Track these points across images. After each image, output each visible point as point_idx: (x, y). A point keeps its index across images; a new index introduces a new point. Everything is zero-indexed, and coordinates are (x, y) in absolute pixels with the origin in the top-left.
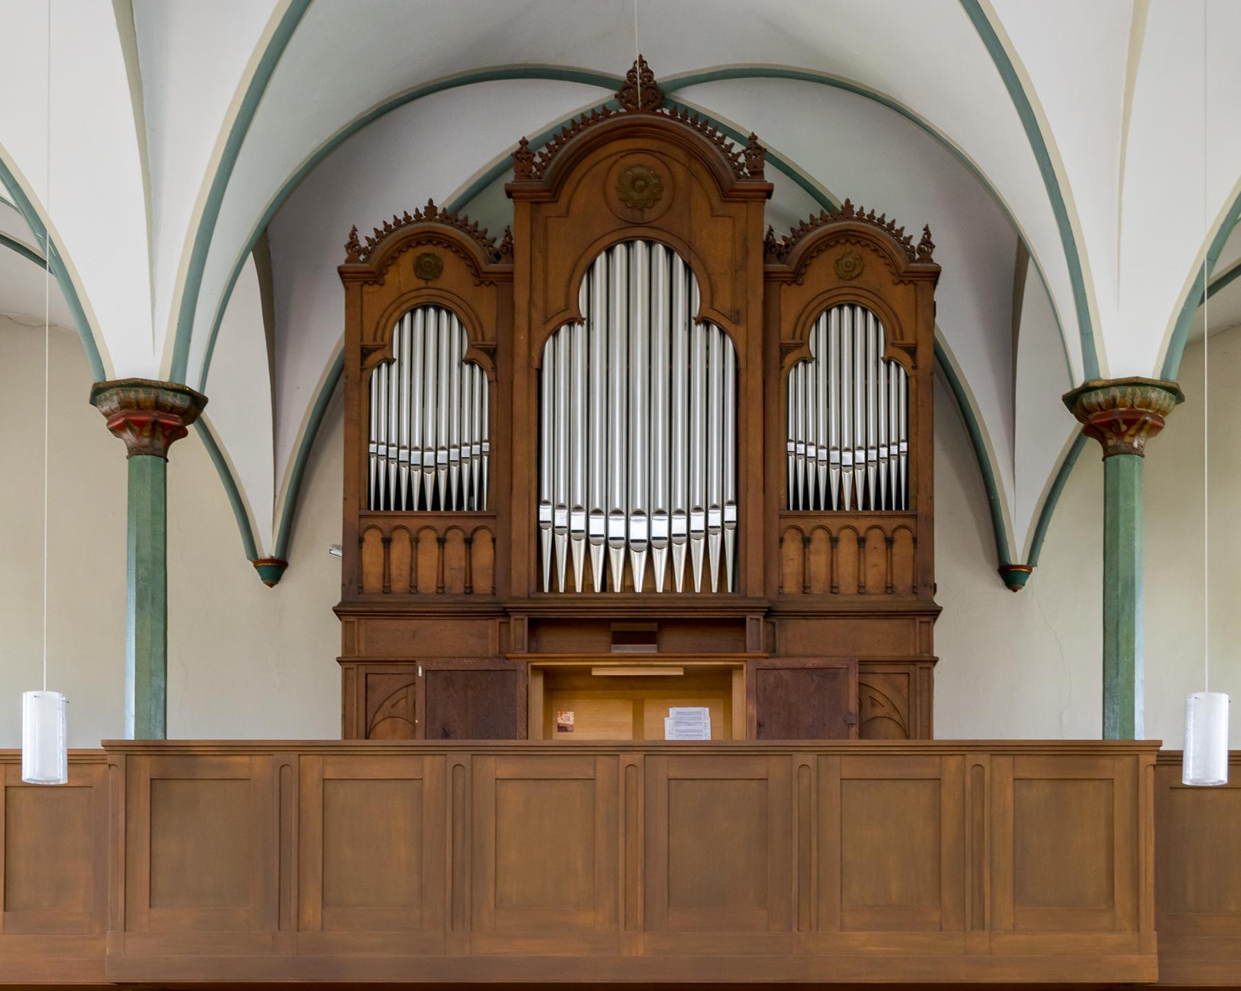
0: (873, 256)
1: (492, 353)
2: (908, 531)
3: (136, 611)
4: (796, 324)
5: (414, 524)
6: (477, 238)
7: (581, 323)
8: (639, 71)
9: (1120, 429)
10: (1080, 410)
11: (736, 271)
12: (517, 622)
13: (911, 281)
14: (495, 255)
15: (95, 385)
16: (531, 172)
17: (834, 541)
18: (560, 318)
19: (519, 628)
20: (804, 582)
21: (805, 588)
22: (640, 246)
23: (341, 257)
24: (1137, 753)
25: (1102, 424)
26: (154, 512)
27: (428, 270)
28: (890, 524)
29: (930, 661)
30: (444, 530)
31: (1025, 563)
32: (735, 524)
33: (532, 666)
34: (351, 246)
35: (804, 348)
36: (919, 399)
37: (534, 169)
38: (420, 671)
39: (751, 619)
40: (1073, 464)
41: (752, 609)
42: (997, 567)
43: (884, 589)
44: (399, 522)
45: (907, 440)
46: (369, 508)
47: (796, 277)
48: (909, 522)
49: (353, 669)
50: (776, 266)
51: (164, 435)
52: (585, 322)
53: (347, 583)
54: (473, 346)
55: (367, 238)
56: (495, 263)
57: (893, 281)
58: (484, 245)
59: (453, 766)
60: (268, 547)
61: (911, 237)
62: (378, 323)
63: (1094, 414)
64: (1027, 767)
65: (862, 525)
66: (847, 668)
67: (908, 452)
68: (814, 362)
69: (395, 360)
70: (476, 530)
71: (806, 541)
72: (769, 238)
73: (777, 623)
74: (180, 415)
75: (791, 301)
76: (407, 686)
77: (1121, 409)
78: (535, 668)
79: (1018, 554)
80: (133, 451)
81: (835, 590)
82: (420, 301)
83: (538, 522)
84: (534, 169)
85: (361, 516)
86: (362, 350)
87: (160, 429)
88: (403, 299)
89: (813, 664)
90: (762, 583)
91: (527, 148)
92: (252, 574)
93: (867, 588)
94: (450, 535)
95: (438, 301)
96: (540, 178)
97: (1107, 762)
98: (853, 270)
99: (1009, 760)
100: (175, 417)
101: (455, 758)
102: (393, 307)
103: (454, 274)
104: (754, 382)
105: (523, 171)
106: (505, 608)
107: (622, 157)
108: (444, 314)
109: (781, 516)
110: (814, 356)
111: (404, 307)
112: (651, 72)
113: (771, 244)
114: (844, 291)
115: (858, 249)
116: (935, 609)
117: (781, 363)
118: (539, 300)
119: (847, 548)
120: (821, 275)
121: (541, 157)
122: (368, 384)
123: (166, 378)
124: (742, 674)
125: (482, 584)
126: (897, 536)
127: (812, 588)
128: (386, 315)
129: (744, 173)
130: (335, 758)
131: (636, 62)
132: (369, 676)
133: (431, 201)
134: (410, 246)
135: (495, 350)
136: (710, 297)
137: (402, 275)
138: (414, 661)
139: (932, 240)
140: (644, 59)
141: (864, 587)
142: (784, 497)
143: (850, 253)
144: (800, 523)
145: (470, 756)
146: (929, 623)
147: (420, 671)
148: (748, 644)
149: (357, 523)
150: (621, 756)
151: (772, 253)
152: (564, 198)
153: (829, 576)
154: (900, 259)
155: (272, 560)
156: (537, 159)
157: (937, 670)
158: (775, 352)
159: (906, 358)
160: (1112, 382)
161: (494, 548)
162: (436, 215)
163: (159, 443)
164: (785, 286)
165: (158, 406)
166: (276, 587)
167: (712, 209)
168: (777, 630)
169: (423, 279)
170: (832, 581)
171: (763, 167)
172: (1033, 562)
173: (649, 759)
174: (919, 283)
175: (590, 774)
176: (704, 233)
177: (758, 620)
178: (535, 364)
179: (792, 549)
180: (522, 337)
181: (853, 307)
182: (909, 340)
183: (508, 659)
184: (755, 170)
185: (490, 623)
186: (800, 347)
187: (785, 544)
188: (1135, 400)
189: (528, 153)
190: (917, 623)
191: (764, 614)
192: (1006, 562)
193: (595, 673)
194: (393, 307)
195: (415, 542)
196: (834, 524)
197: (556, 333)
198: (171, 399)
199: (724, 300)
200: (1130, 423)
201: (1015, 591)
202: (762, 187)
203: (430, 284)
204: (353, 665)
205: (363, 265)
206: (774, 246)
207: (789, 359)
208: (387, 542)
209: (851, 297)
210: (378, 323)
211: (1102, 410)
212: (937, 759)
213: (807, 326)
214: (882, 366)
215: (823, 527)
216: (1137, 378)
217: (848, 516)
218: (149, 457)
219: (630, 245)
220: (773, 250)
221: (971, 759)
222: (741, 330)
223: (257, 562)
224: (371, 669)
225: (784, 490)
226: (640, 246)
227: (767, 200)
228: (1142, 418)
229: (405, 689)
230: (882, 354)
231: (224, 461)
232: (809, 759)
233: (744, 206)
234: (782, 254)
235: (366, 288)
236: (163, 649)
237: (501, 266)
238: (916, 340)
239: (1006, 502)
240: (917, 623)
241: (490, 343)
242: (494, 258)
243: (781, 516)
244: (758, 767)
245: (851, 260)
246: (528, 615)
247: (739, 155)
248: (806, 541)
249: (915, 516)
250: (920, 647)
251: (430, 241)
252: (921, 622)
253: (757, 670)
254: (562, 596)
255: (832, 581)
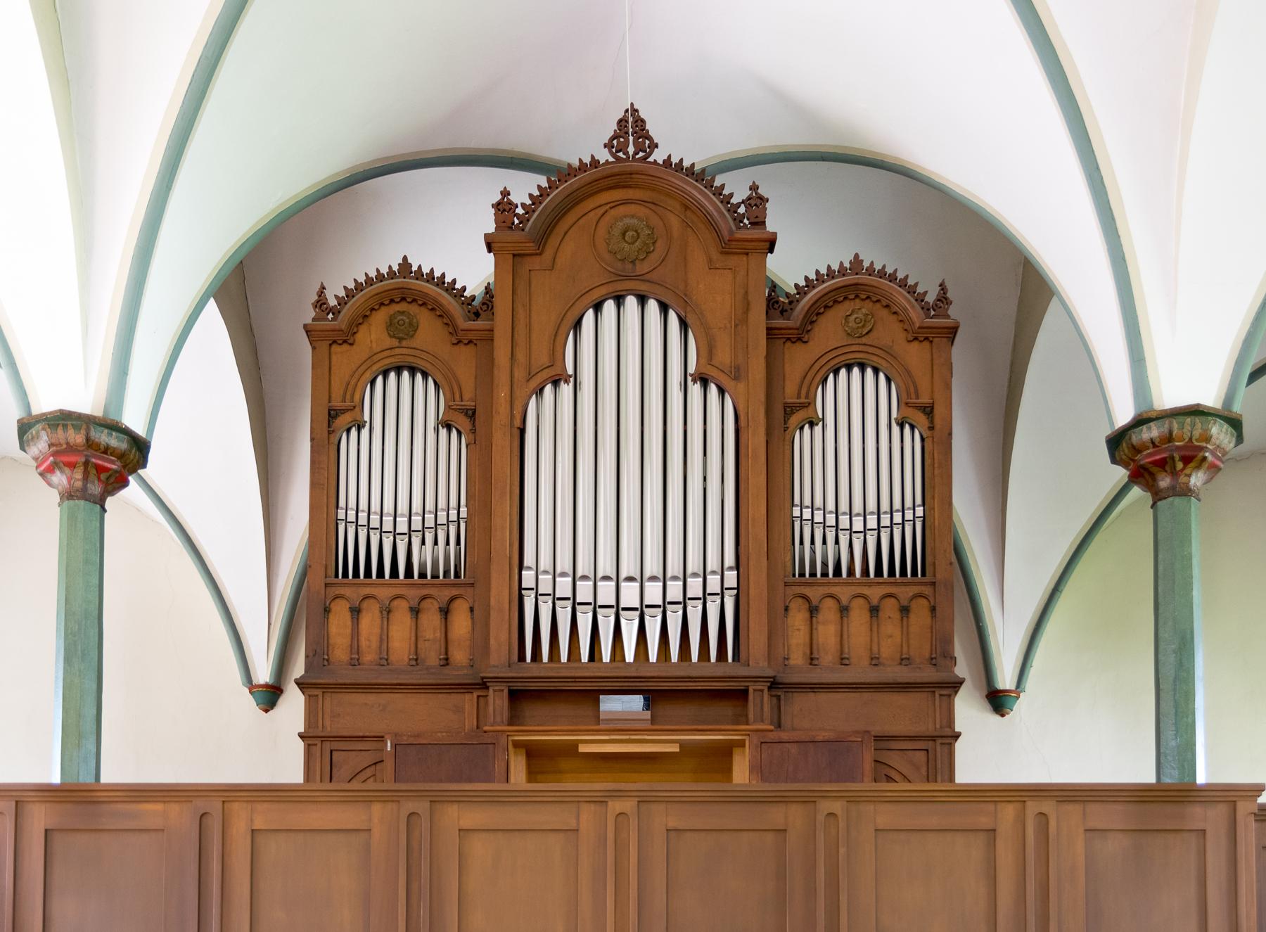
0: (885, 312)
1: (471, 414)
2: (925, 600)
3: (64, 668)
4: (802, 383)
5: (384, 593)
6: (455, 296)
7: (567, 382)
8: (631, 119)
9: (1175, 467)
10: (1126, 451)
11: (736, 326)
12: (496, 693)
13: (926, 338)
14: (474, 313)
15: (19, 421)
16: (513, 223)
17: (844, 610)
18: (546, 374)
19: (497, 701)
20: (811, 653)
21: (812, 660)
22: (631, 302)
23: (309, 314)
24: (1234, 799)
25: (1155, 463)
26: (87, 562)
27: (401, 330)
28: (905, 593)
29: (952, 737)
30: (417, 600)
31: (1013, 688)
32: (735, 591)
33: (513, 741)
34: (318, 306)
35: (810, 408)
36: (936, 461)
37: (516, 221)
38: (389, 744)
39: (755, 690)
40: (1062, 590)
41: (756, 679)
42: (985, 693)
43: (899, 661)
44: (367, 591)
45: (924, 504)
46: (337, 576)
47: (800, 336)
48: (927, 590)
49: (316, 745)
50: (779, 322)
51: (99, 479)
52: (572, 379)
53: (311, 654)
54: (449, 406)
55: (336, 297)
56: (474, 321)
57: (907, 338)
58: (463, 304)
59: (408, 813)
60: (263, 674)
61: (926, 293)
62: (348, 384)
63: (1145, 453)
64: (1101, 816)
65: (875, 593)
66: (862, 741)
67: (924, 517)
68: (821, 424)
69: (366, 422)
70: (452, 599)
71: (813, 611)
72: (771, 294)
73: (782, 697)
74: (118, 459)
75: (797, 359)
76: (375, 764)
77: (1177, 444)
78: (517, 745)
79: (1005, 679)
80: (68, 495)
81: (846, 662)
82: (394, 361)
83: (520, 589)
84: (516, 221)
85: (326, 585)
86: (329, 411)
87: (95, 472)
88: (376, 358)
89: (824, 736)
90: (766, 653)
91: (508, 199)
92: (248, 702)
93: (881, 660)
94: (425, 604)
95: (412, 361)
96: (523, 230)
97: (1197, 810)
98: (863, 326)
99: (1077, 808)
100: (111, 459)
101: (409, 806)
102: (363, 368)
103: (429, 333)
104: (756, 440)
105: (504, 222)
106: (483, 678)
107: (611, 208)
108: (419, 377)
109: (786, 584)
110: (821, 416)
111: (375, 368)
112: (643, 121)
113: (774, 300)
114: (853, 348)
115: (867, 307)
116: (957, 680)
117: (785, 424)
118: (521, 356)
119: (859, 616)
120: (829, 332)
121: (523, 208)
122: (336, 447)
123: (99, 413)
124: (744, 752)
125: (459, 656)
126: (914, 605)
127: (821, 660)
128: (357, 376)
129: (745, 224)
130: (266, 805)
131: (627, 111)
132: (334, 753)
133: (405, 258)
134: (382, 304)
135: (474, 411)
136: (708, 352)
137: (374, 335)
138: (383, 737)
139: (949, 295)
140: (635, 107)
141: (878, 658)
142: (789, 564)
143: (859, 309)
144: (807, 591)
145: (428, 805)
146: (949, 696)
147: (389, 744)
148: (751, 716)
149: (323, 592)
150: (610, 804)
151: (775, 309)
152: (549, 253)
153: (839, 647)
154: (916, 315)
155: (266, 686)
156: (520, 211)
157: (959, 746)
158: (779, 413)
159: (921, 419)
160: (1169, 411)
161: (472, 618)
162: (411, 273)
163: (95, 488)
164: (788, 344)
165: (90, 444)
166: (271, 712)
167: (710, 261)
168: (782, 702)
169: (395, 338)
170: (842, 652)
171: (765, 218)
172: (1022, 686)
173: (644, 807)
174: (936, 339)
175: (573, 825)
176: (701, 286)
177: (762, 691)
178: (518, 423)
179: (798, 618)
180: (502, 394)
181: (863, 368)
182: (925, 400)
183: (485, 732)
184: (756, 220)
185: (467, 696)
186: (807, 407)
187: (791, 613)
188: (1194, 433)
189: (510, 204)
190: (937, 696)
191: (769, 684)
192: (994, 686)
193: (583, 749)
194: (363, 368)
195: (387, 612)
196: (844, 593)
197: (540, 392)
198: (104, 438)
199: (724, 356)
200: (1187, 460)
201: (1003, 716)
202: (765, 236)
203: (404, 343)
204: (318, 742)
205: (332, 323)
206: (777, 302)
207: (794, 420)
208: (356, 612)
209: (861, 355)
210: (348, 384)
211: (1154, 445)
212: (991, 807)
213: (812, 390)
214: (896, 429)
215: (831, 596)
216: (1198, 405)
217: (860, 584)
218: (82, 502)
219: (621, 300)
220: (776, 306)
221: (1033, 807)
222: (741, 386)
223: (252, 686)
224: (336, 745)
225: (789, 557)
226: (631, 302)
227: (769, 254)
228: (1201, 454)
229: (374, 766)
230: (894, 414)
231: (201, 556)
232: (837, 807)
233: (745, 258)
234: (786, 311)
235: (335, 347)
236: (95, 712)
237: (480, 324)
238: (932, 399)
239: (994, 628)
240: (937, 696)
241: (468, 403)
242: (473, 315)
243: (786, 584)
244: (776, 815)
245: (860, 316)
246: (509, 686)
247: (738, 205)
248: (813, 611)
249: (933, 584)
250: (941, 722)
251: (403, 299)
252: (941, 695)
253: (762, 743)
254: (546, 665)
255: (842, 652)
